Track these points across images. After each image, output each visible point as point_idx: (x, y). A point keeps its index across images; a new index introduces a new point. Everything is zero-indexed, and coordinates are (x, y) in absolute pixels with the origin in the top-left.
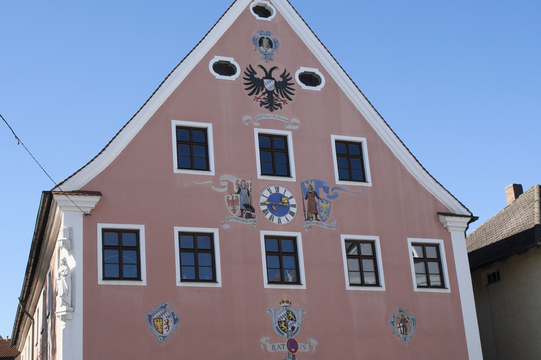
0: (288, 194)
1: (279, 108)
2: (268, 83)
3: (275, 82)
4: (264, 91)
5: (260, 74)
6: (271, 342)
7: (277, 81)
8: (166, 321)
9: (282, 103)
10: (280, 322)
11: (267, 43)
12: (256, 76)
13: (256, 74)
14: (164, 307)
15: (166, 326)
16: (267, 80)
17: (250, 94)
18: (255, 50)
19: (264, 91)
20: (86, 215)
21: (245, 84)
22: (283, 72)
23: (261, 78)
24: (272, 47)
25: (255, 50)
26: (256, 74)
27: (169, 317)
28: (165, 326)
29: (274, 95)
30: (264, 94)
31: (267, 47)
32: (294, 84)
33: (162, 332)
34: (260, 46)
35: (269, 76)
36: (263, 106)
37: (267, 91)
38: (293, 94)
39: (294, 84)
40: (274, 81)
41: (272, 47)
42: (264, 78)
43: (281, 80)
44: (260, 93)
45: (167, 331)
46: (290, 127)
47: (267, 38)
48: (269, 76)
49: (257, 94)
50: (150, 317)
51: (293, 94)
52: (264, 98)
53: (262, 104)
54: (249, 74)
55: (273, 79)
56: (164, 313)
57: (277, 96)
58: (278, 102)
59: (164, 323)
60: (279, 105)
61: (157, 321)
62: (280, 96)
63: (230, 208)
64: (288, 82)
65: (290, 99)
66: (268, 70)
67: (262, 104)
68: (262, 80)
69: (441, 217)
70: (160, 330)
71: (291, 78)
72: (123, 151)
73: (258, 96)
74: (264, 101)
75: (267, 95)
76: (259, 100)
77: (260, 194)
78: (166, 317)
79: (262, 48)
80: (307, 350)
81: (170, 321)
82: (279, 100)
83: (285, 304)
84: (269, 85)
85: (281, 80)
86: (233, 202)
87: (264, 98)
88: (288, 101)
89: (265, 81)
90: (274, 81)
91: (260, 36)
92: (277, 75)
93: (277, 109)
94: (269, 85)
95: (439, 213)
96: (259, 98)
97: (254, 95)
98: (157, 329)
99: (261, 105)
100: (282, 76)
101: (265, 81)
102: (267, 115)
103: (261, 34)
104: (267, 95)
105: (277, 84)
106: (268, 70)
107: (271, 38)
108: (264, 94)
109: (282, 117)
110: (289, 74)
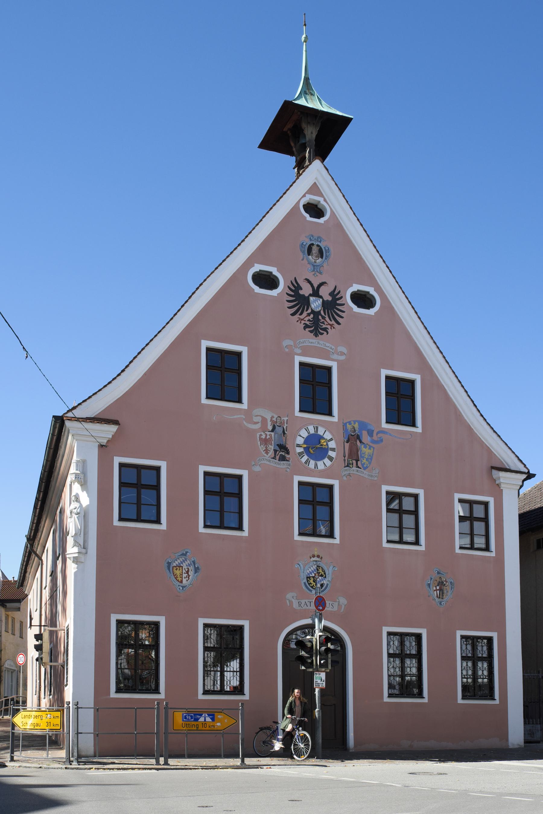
0: (328, 436)
1: (325, 333)
2: (315, 301)
3: (323, 300)
4: (309, 311)
5: (306, 290)
7: (325, 299)
8: (186, 570)
9: (329, 327)
10: (308, 578)
11: (317, 251)
12: (301, 292)
13: (301, 289)
14: (184, 555)
15: (186, 575)
16: (314, 298)
17: (293, 314)
19: (309, 311)
20: (101, 446)
21: (288, 301)
22: (332, 289)
23: (307, 295)
24: (322, 257)
26: (301, 289)
27: (189, 565)
28: (185, 575)
29: (320, 317)
30: (309, 315)
31: (316, 257)
32: (344, 304)
33: (181, 582)
34: (309, 255)
35: (316, 293)
36: (307, 329)
37: (313, 312)
38: (342, 317)
39: (344, 304)
40: (321, 300)
41: (322, 257)
42: (310, 295)
43: (330, 299)
44: (305, 314)
45: (187, 580)
46: (335, 357)
47: (318, 246)
48: (316, 293)
49: (301, 314)
51: (342, 317)
52: (309, 320)
53: (306, 327)
54: (293, 288)
55: (321, 297)
56: (184, 561)
57: (324, 318)
58: (324, 326)
59: (184, 571)
60: (325, 330)
61: (176, 569)
62: (327, 319)
63: (262, 448)
64: (338, 302)
65: (339, 323)
66: (316, 286)
67: (306, 327)
68: (308, 297)
69: (494, 472)
70: (180, 579)
71: (342, 297)
73: (302, 317)
74: (308, 323)
75: (312, 316)
76: (303, 322)
78: (187, 566)
79: (310, 257)
81: (190, 570)
82: (326, 323)
83: (316, 559)
84: (316, 304)
85: (330, 299)
86: (265, 442)
87: (309, 320)
88: (336, 325)
89: (312, 299)
90: (321, 300)
91: (309, 243)
92: (325, 292)
93: (322, 334)
94: (316, 304)
96: (303, 320)
97: (297, 316)
98: (176, 578)
99: (305, 328)
100: (332, 294)
101: (312, 299)
102: (311, 340)
103: (311, 240)
104: (312, 316)
105: (325, 304)
106: (316, 286)
107: (322, 245)
108: (309, 315)
109: (328, 344)
110: (339, 292)
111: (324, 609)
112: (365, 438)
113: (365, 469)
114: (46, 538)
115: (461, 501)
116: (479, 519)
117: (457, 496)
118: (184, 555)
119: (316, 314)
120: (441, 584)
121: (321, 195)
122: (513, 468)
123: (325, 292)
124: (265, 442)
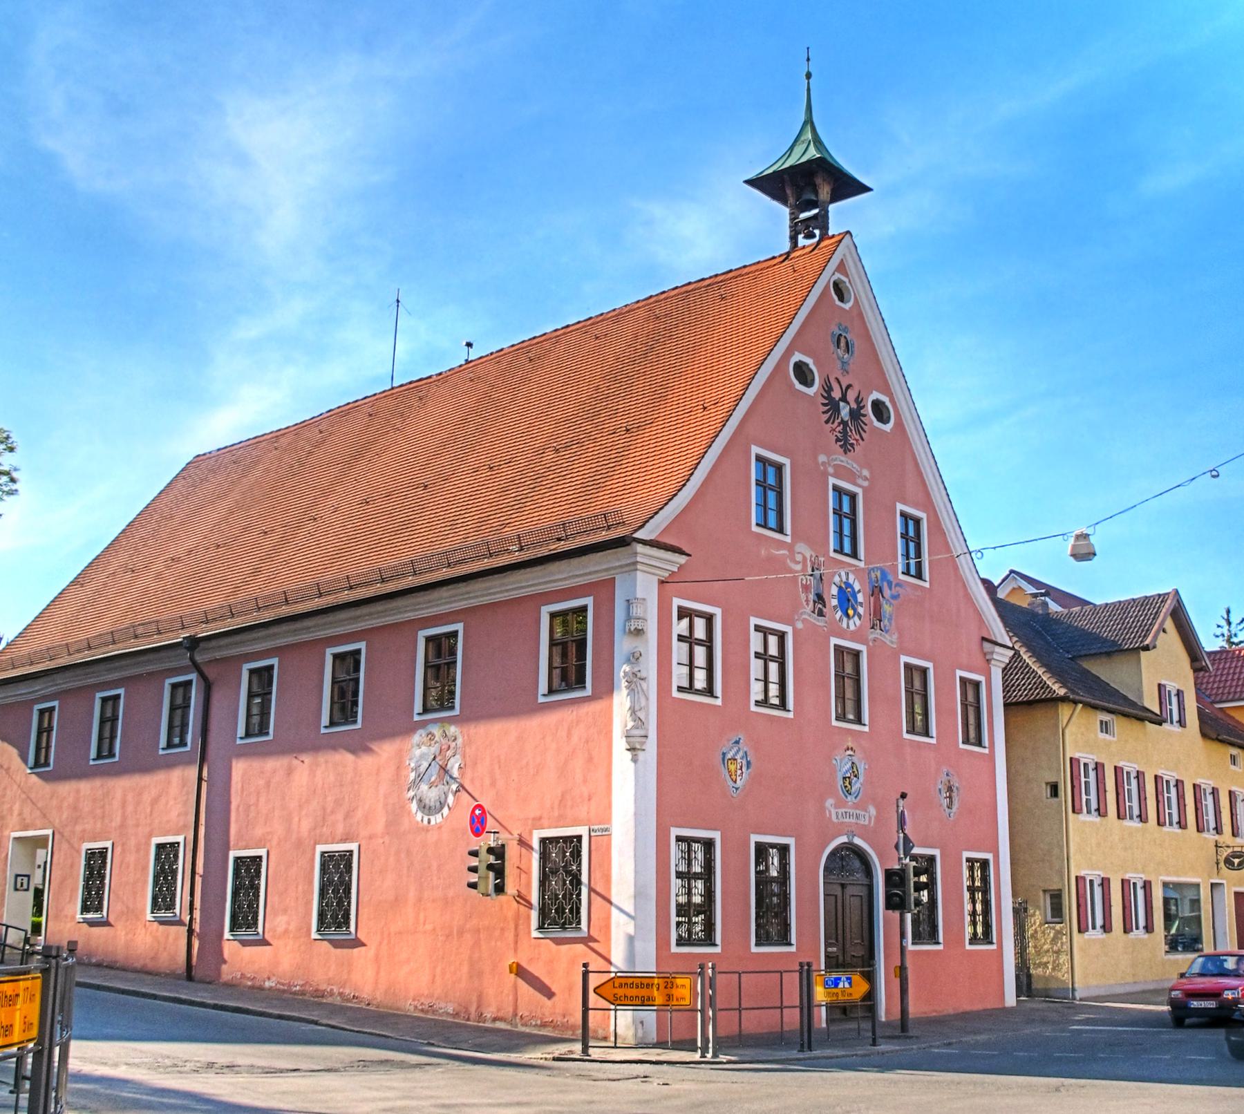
0: (857, 587)
6: (836, 807)
10: (844, 778)
14: (737, 742)
17: (827, 422)
18: (849, 386)
20: (662, 582)
25: (849, 386)
35: (844, 398)
46: (860, 481)
50: (724, 754)
53: (838, 440)
60: (852, 445)
63: (803, 596)
69: (987, 645)
72: (256, 441)
77: (831, 583)
80: (866, 823)
83: (850, 752)
84: (845, 412)
86: (806, 588)
94: (845, 412)
95: (984, 639)
97: (830, 425)
101: (842, 404)
111: (473, 811)
112: (887, 592)
113: (887, 632)
114: (151, 656)
115: (758, 628)
116: (700, 642)
117: (754, 621)
118: (737, 742)
119: (844, 423)
120: (950, 789)
121: (847, 276)
122: (1000, 641)
123: (851, 396)
124: (806, 588)
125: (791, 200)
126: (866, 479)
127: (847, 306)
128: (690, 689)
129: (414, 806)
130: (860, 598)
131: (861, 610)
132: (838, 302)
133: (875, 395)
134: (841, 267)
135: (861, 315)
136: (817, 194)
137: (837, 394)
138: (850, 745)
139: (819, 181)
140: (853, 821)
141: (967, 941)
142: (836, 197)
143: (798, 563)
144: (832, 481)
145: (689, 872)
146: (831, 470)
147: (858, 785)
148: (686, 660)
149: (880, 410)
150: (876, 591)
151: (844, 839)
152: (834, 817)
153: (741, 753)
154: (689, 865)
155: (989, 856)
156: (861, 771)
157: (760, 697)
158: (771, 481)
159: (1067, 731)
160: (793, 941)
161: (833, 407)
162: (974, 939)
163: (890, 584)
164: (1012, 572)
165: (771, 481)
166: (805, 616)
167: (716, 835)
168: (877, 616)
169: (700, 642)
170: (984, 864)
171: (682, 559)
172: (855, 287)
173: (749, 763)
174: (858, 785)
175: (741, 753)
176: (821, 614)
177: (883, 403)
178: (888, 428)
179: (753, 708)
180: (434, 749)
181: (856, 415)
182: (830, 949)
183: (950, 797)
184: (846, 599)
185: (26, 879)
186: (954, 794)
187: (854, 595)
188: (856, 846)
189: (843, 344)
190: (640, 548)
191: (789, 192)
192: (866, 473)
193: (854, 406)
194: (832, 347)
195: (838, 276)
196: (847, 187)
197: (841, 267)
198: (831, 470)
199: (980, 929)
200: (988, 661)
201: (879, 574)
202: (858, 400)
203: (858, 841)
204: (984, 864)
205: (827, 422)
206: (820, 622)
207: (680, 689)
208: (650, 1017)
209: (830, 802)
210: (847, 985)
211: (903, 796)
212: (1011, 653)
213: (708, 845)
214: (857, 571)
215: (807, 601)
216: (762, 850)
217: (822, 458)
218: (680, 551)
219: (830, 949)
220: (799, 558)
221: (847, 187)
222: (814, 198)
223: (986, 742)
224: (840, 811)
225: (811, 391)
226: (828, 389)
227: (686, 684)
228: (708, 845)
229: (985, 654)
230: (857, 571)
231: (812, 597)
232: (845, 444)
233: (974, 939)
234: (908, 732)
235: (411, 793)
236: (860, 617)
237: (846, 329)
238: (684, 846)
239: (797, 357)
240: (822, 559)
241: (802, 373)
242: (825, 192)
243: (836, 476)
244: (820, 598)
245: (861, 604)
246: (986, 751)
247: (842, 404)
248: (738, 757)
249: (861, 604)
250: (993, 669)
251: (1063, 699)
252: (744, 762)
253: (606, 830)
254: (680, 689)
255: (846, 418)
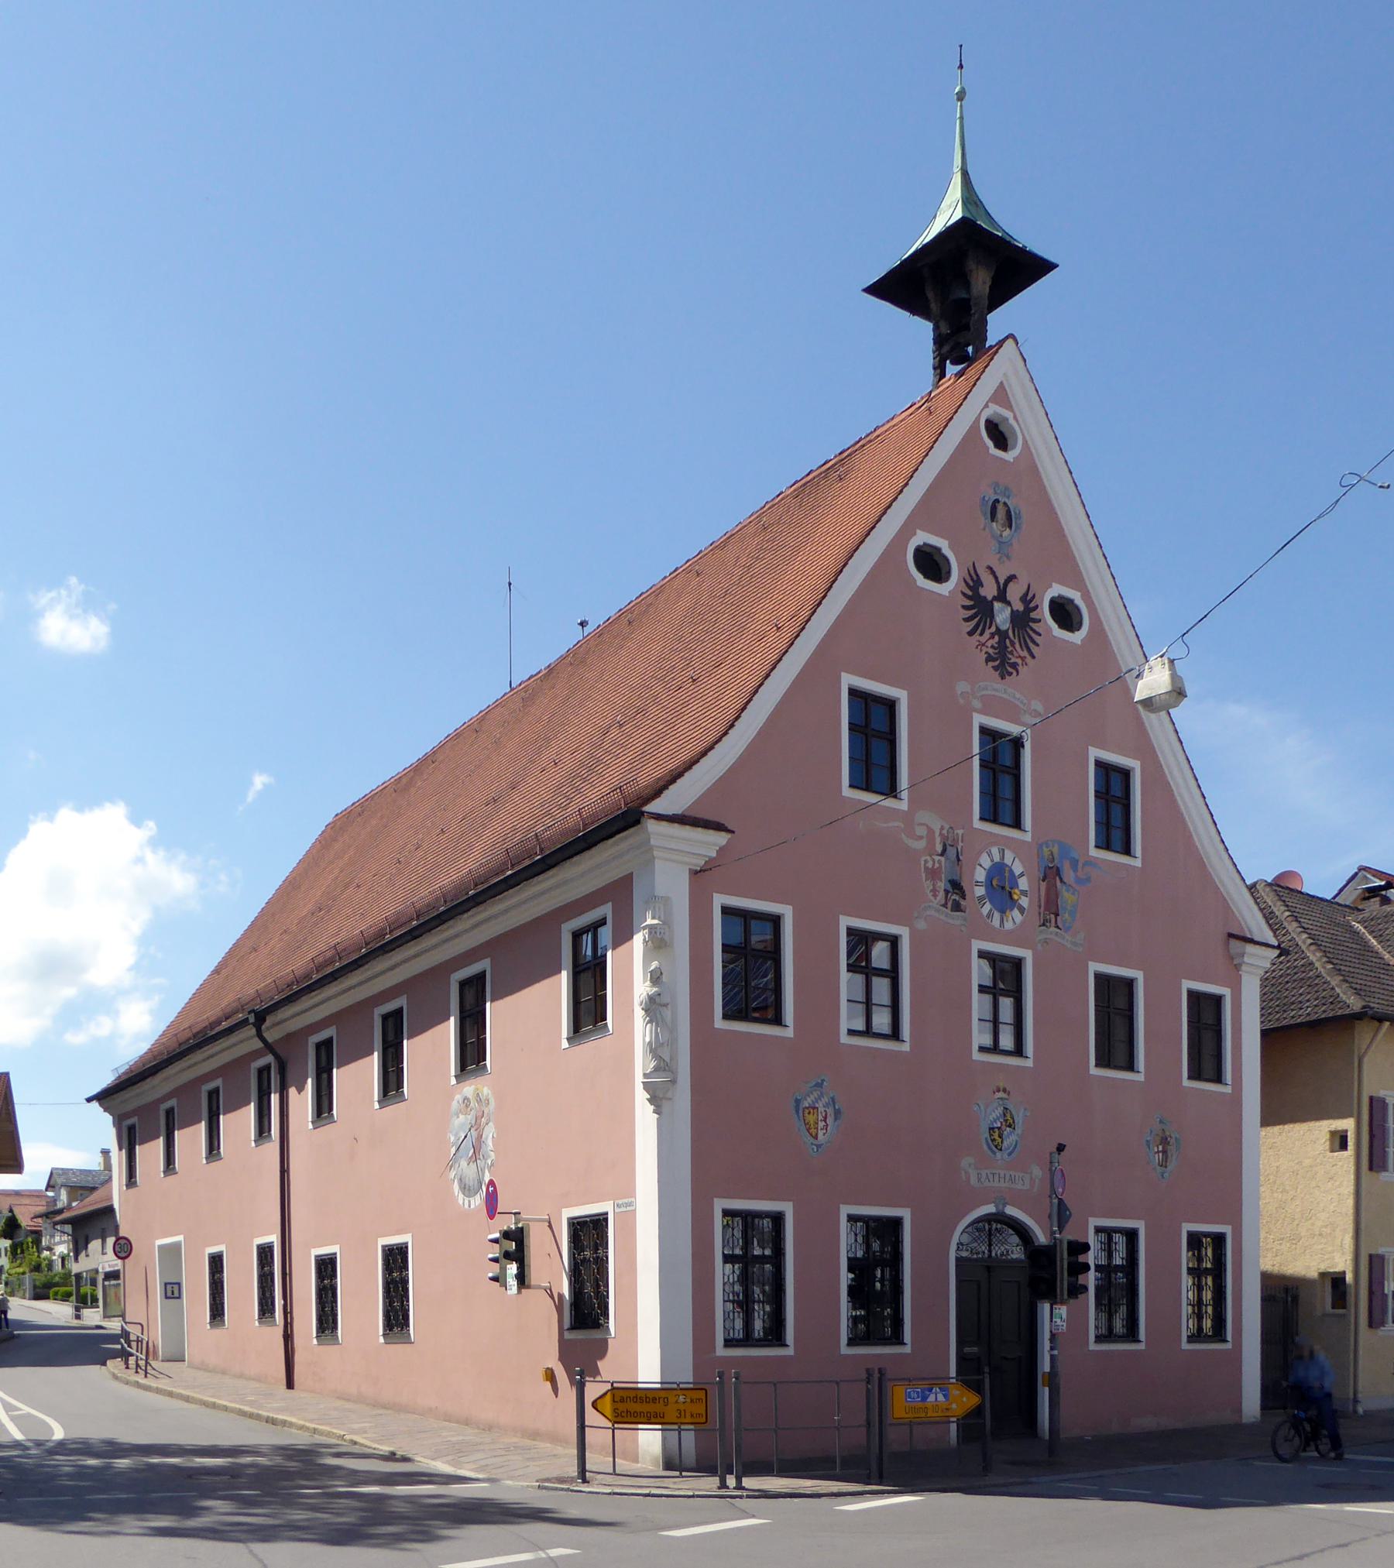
0: (1018, 869)
4: (993, 629)
9: (1019, 661)
10: (992, 1129)
14: (819, 1085)
17: (971, 634)
18: (1011, 578)
19: (993, 629)
20: (695, 873)
24: (1010, 527)
25: (1011, 578)
30: (992, 636)
35: (1002, 596)
41: (1010, 527)
50: (798, 1102)
57: (1013, 644)
58: (1013, 660)
60: (1014, 666)
63: (928, 885)
73: (983, 639)
74: (991, 651)
75: (997, 638)
80: (1027, 1187)
83: (1001, 1095)
84: (1002, 616)
86: (933, 874)
88: (1029, 659)
93: (1010, 674)
94: (1002, 616)
95: (1231, 936)
97: (976, 637)
99: (987, 661)
101: (997, 605)
112: (1069, 875)
113: (1067, 930)
115: (982, 954)
118: (819, 1085)
120: (1164, 1141)
123: (1014, 593)
124: (933, 874)
125: (934, 307)
126: (1037, 714)
127: (1009, 456)
128: (995, 1049)
129: (456, 1187)
130: (1023, 884)
131: (1024, 902)
132: (994, 451)
133: (1057, 590)
134: (1001, 395)
135: (1033, 471)
136: (967, 285)
137: (989, 590)
138: (1001, 1085)
139: (971, 264)
140: (1015, 1189)
141: (1184, 1339)
142: (1001, 293)
143: (921, 838)
144: (978, 720)
145: (1109, 1265)
146: (977, 704)
147: (1013, 1138)
148: (989, 1016)
149: (1065, 614)
150: (1051, 874)
151: (990, 1209)
152: (973, 1181)
153: (825, 1099)
154: (1110, 1256)
155: (1226, 1229)
156: (1019, 1120)
157: (988, 1041)
158: (873, 721)
159: (1366, 1060)
160: (1229, 1337)
161: (980, 610)
162: (1197, 1336)
163: (1074, 864)
164: (1362, 869)
165: (873, 721)
166: (933, 913)
167: (1140, 1225)
168: (1051, 909)
169: (880, 972)
170: (1219, 1240)
171: (722, 838)
172: (1027, 425)
173: (837, 1114)
174: (1013, 1138)
175: (825, 1099)
176: (957, 907)
177: (1071, 601)
178: (1077, 637)
179: (977, 1056)
180: (471, 1118)
181: (1023, 620)
182: (967, 1350)
183: (1164, 1152)
184: (1001, 887)
185: (176, 1287)
186: (1171, 1149)
187: (1014, 881)
188: (1011, 1218)
189: (1001, 513)
190: (651, 825)
191: (930, 295)
192: (1037, 705)
193: (1019, 606)
194: (983, 520)
195: (994, 410)
196: (1018, 268)
197: (1001, 395)
198: (977, 704)
199: (1207, 1324)
200: (1238, 967)
201: (1055, 850)
202: (1026, 599)
203: (1011, 1211)
204: (1219, 1240)
205: (971, 634)
206: (956, 919)
207: (982, 1049)
208: (689, 1438)
209: (966, 1162)
210: (941, 1397)
211: (1061, 1148)
212: (1277, 952)
213: (1131, 1235)
214: (1018, 847)
215: (934, 892)
216: (1195, 1241)
217: (962, 687)
218: (719, 827)
219: (967, 1350)
220: (921, 831)
221: (1018, 268)
222: (964, 295)
223: (1228, 1076)
224: (984, 1173)
225: (944, 589)
226: (973, 583)
227: (860, 1025)
228: (1131, 1235)
229: (1232, 959)
230: (1018, 847)
231: (942, 885)
232: (1002, 664)
233: (1197, 1336)
234: (1190, 1078)
235: (452, 1174)
236: (1022, 910)
237: (1007, 492)
238: (1103, 1237)
239: (921, 538)
240: (960, 832)
241: (931, 564)
242: (981, 281)
243: (983, 712)
244: (956, 886)
245: (1024, 893)
246: (1228, 1090)
247: (997, 605)
248: (820, 1105)
249: (1024, 893)
250: (1245, 978)
251: (1358, 1017)
252: (830, 1111)
253: (630, 1204)
254: (982, 1049)
255: (1004, 627)
